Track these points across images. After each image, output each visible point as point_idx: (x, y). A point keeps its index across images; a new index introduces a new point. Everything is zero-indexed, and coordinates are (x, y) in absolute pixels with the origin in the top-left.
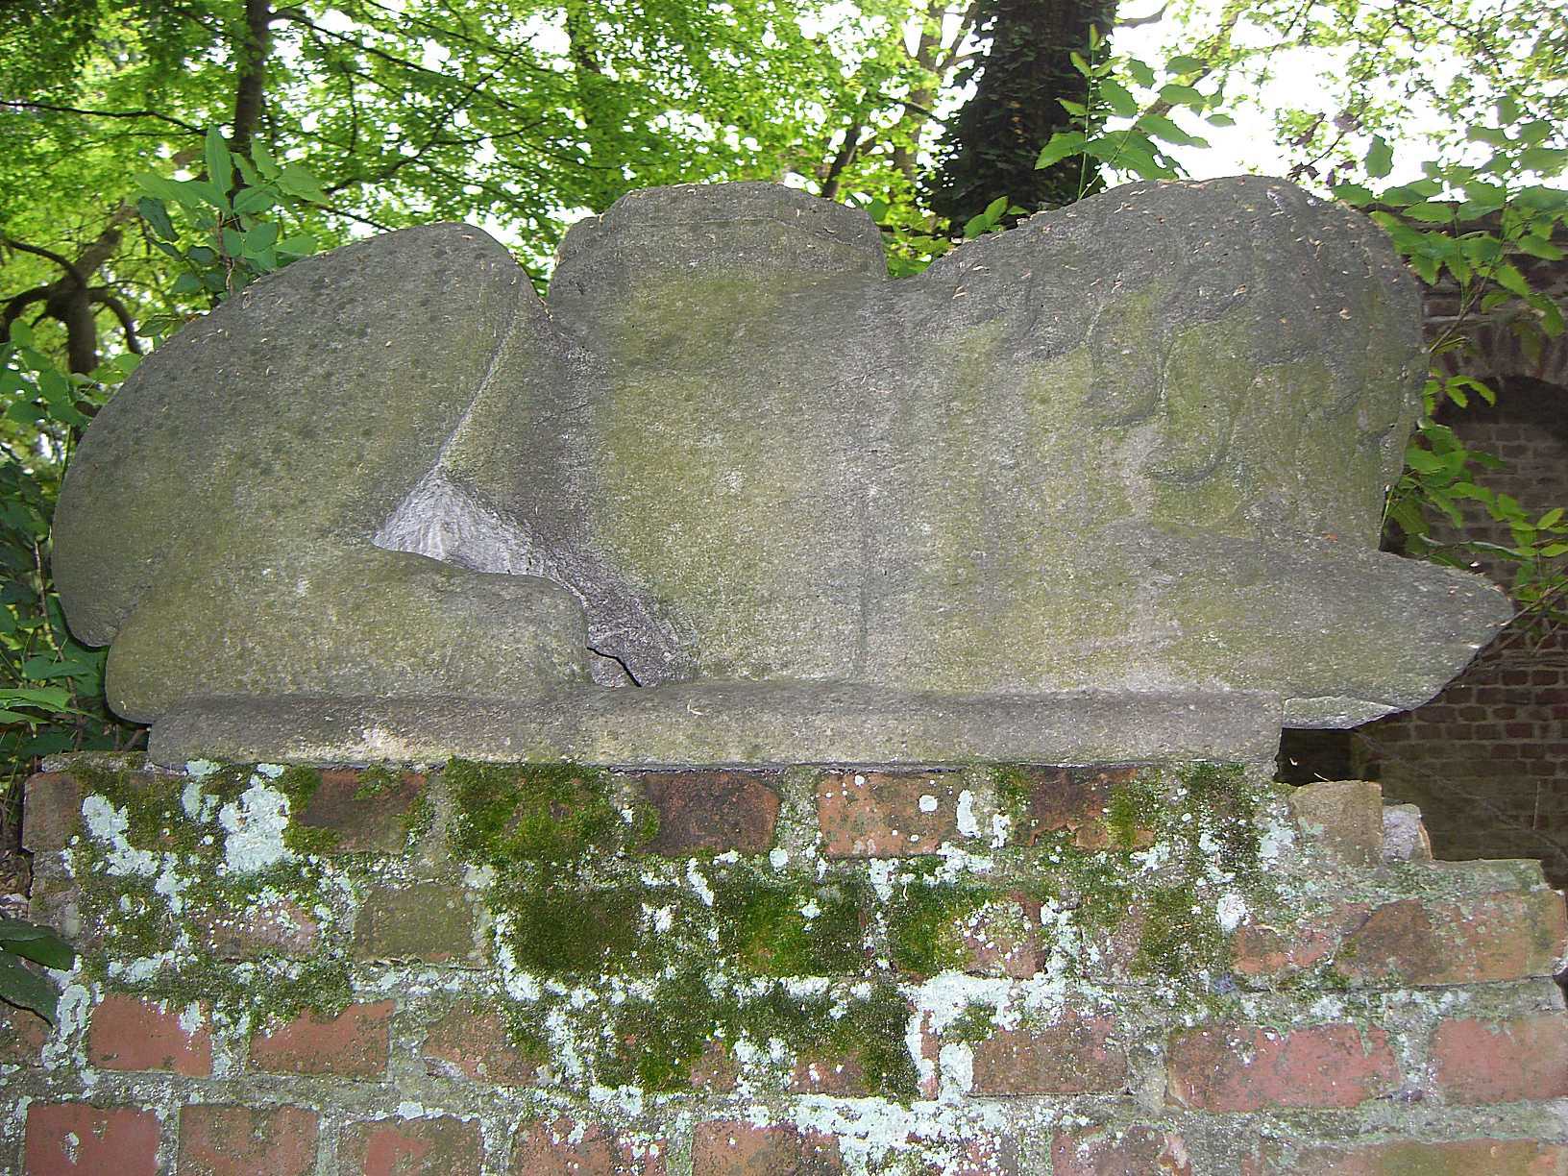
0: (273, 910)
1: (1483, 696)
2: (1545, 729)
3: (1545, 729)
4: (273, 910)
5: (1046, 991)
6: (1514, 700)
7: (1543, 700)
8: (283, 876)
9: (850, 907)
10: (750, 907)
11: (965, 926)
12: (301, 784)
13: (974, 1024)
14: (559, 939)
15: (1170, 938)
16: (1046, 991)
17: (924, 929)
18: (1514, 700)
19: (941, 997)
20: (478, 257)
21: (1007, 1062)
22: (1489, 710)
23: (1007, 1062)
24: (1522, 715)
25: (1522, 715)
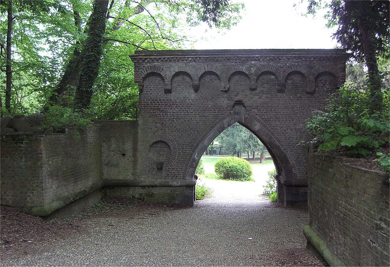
0: (5, 139)
1: (150, 109)
2: (158, 112)
3: (158, 112)
4: (5, 139)
5: (27, 141)
6: (154, 109)
7: (157, 109)
8: (5, 138)
9: (22, 139)
10: (19, 139)
11: (25, 140)
12: (5, 135)
13: (25, 142)
14: (13, 140)
15: (31, 140)
16: (27, 141)
17: (23, 140)
18: (154, 109)
19: (24, 142)
20: (13, 155)
21: (26, 144)
22: (151, 110)
23: (26, 144)
24: (155, 111)
25: (155, 111)
